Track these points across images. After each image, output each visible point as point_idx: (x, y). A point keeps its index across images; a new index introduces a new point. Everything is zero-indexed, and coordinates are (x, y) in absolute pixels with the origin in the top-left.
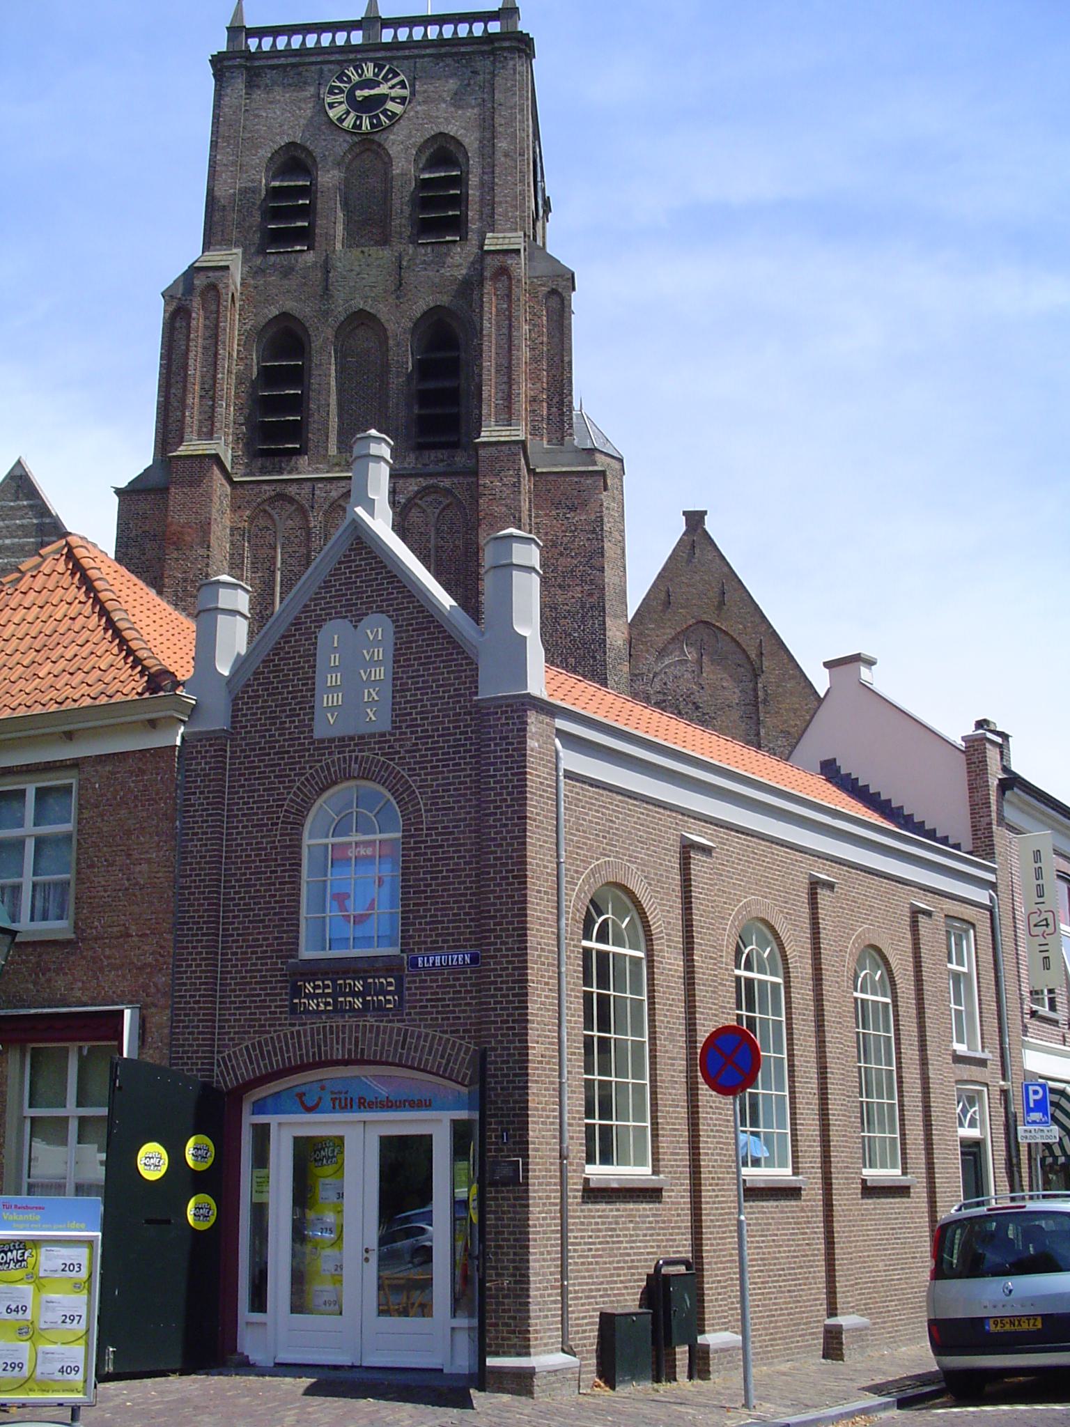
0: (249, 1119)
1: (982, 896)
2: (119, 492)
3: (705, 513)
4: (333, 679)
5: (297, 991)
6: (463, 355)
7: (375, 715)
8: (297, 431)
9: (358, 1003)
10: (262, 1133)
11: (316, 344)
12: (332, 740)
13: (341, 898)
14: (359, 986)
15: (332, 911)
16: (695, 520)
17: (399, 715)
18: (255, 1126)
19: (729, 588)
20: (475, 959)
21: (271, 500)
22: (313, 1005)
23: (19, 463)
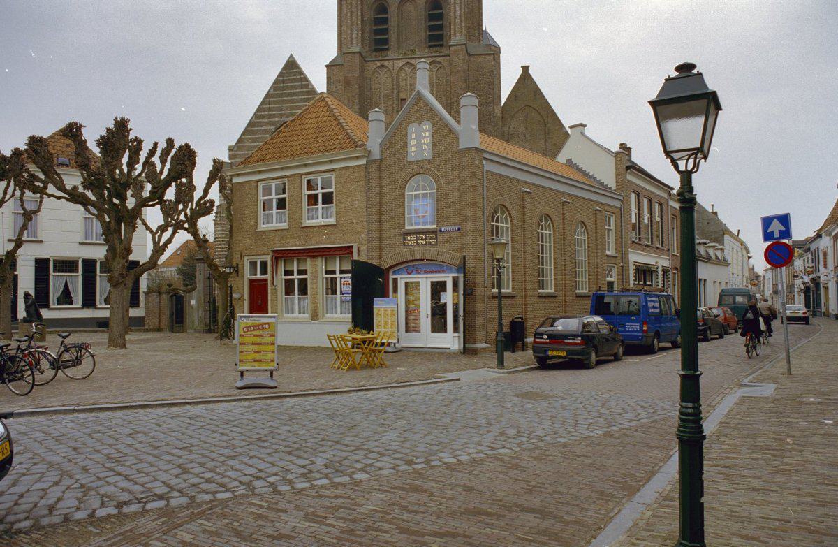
0: (391, 277)
1: (617, 204)
2: (326, 66)
3: (528, 66)
4: (413, 142)
5: (405, 239)
6: (444, 23)
7: (427, 154)
8: (386, 41)
9: (424, 242)
10: (395, 281)
11: (392, 9)
12: (413, 162)
13: (416, 211)
14: (424, 237)
15: (414, 215)
16: (525, 69)
17: (434, 154)
18: (393, 279)
19: (537, 92)
20: (459, 229)
21: (379, 67)
22: (410, 243)
23: (291, 56)
